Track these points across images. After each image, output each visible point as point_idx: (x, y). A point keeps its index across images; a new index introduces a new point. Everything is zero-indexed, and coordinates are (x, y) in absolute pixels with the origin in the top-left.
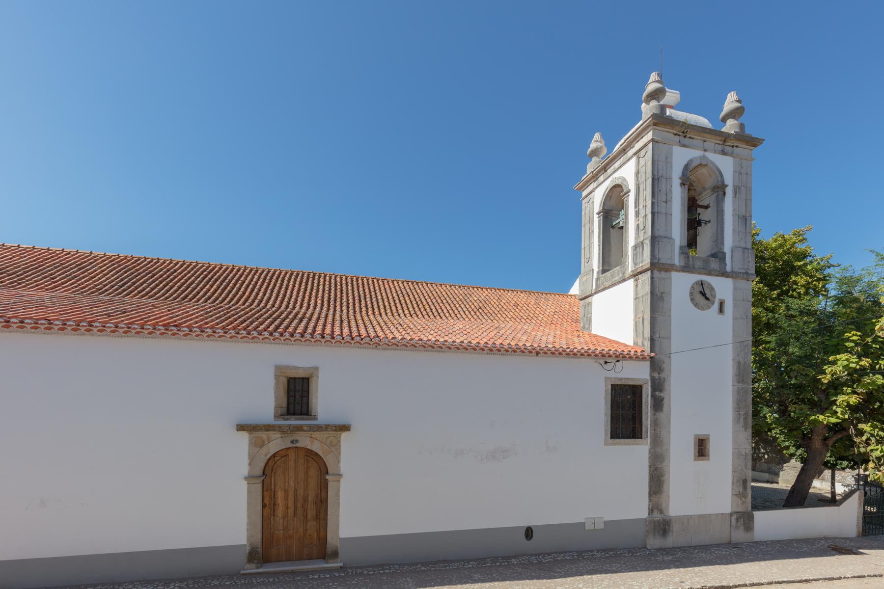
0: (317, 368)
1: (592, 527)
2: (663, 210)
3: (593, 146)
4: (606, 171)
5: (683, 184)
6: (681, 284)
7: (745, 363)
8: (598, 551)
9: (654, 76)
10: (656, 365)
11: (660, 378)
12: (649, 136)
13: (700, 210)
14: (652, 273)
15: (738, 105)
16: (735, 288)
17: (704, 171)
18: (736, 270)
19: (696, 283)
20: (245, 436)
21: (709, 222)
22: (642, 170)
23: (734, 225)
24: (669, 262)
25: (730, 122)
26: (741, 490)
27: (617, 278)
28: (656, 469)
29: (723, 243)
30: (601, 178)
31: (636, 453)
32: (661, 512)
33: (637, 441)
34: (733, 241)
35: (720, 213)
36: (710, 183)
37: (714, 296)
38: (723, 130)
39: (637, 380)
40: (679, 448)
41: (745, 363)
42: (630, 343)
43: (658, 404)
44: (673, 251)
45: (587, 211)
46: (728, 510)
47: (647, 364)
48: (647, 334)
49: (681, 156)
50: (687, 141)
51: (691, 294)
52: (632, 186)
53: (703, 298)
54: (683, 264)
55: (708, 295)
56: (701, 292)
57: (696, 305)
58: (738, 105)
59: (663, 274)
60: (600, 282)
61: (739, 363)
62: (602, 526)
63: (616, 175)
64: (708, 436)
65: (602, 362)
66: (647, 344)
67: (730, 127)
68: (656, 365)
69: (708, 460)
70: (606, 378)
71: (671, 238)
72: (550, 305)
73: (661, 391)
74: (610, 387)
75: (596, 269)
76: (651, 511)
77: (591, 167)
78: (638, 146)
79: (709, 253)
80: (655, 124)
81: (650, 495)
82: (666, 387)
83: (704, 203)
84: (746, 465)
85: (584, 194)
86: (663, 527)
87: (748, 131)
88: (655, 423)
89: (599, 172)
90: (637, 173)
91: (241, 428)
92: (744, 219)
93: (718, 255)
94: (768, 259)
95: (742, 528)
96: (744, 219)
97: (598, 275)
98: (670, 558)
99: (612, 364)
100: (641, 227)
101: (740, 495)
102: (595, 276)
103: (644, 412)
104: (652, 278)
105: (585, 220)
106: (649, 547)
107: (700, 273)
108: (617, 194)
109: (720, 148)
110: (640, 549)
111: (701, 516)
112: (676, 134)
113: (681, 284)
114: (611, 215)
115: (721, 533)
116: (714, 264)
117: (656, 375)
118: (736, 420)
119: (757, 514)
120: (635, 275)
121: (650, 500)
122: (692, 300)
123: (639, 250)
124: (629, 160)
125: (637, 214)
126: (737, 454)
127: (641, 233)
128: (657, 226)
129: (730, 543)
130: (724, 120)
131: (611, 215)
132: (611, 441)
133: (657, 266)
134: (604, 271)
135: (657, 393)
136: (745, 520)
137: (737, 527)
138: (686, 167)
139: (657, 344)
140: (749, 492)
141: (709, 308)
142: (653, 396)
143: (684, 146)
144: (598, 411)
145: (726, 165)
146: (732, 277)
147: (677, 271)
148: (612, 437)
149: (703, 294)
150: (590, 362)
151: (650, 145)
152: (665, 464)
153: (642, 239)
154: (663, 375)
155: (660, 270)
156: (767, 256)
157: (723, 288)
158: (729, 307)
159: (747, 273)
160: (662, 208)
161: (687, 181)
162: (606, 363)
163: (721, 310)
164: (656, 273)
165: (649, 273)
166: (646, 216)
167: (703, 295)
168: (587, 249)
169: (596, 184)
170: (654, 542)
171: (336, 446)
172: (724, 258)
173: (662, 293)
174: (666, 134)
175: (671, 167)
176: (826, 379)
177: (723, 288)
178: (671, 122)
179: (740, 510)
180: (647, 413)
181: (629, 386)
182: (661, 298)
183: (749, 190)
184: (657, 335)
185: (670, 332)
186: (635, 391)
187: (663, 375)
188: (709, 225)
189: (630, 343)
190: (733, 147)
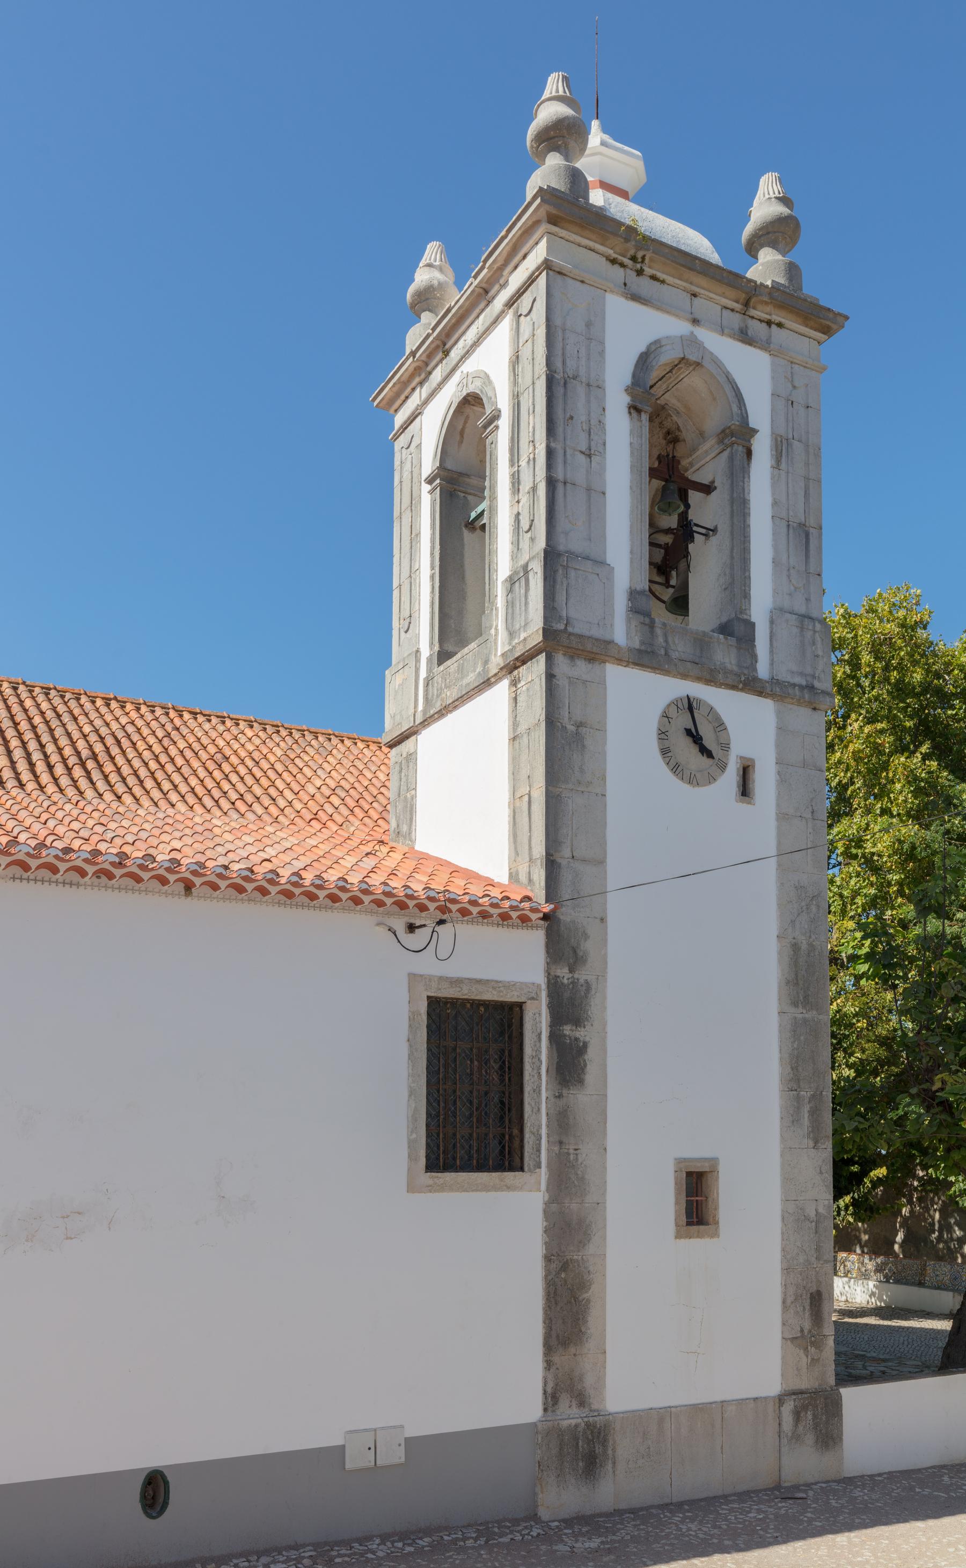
1: (367, 1460)
2: (580, 477)
3: (422, 277)
4: (446, 353)
5: (634, 409)
6: (634, 700)
7: (812, 947)
8: (384, 1538)
9: (554, 84)
10: (564, 942)
11: (574, 983)
12: (538, 254)
13: (694, 497)
14: (549, 660)
15: (782, 210)
16: (782, 729)
17: (693, 381)
18: (784, 676)
19: (675, 703)
21: (714, 530)
22: (526, 353)
23: (775, 547)
24: (596, 632)
25: (767, 255)
26: (807, 1325)
27: (471, 678)
28: (565, 1267)
29: (746, 596)
30: (437, 375)
31: (506, 1215)
32: (582, 1400)
33: (509, 1176)
34: (775, 592)
35: (739, 507)
36: (714, 420)
37: (726, 747)
38: (750, 274)
39: (509, 986)
42: (502, 877)
43: (570, 1063)
44: (608, 601)
45: (406, 475)
46: (772, 1386)
47: (536, 938)
48: (539, 850)
49: (631, 329)
50: (644, 285)
51: (662, 734)
52: (504, 403)
53: (694, 750)
54: (636, 644)
55: (708, 742)
56: (688, 732)
57: (676, 769)
58: (782, 210)
59: (582, 668)
60: (433, 691)
61: (795, 947)
62: (399, 1456)
63: (469, 367)
64: (714, 1162)
65: (399, 925)
66: (539, 875)
67: (766, 268)
68: (564, 942)
69: (715, 1234)
70: (413, 978)
71: (602, 563)
72: (330, 767)
73: (578, 1022)
74: (423, 1007)
75: (425, 652)
76: (551, 1400)
77: (416, 336)
78: (516, 279)
79: (715, 624)
80: (553, 220)
81: (548, 1349)
82: (594, 1009)
83: (703, 477)
84: (818, 1249)
85: (399, 419)
86: (583, 1445)
87: (811, 288)
88: (563, 1122)
89: (430, 355)
90: (515, 360)
92: (802, 536)
93: (737, 630)
94: (955, 695)
95: (810, 1439)
96: (802, 536)
97: (430, 670)
98: (594, 1543)
99: (428, 930)
100: (525, 524)
101: (803, 1340)
102: (423, 674)
103: (528, 1089)
104: (550, 676)
105: (400, 499)
106: (544, 1514)
107: (684, 676)
109: (735, 320)
110: (516, 1522)
111: (698, 1410)
112: (613, 261)
113: (634, 700)
114: (460, 489)
115: (752, 1457)
116: (724, 655)
117: (563, 972)
118: (791, 1117)
119: (849, 1394)
120: (514, 666)
121: (549, 1364)
122: (665, 752)
123: (519, 589)
124: (496, 321)
128: (562, 524)
129: (778, 1487)
130: (752, 249)
131: (460, 489)
132: (428, 1178)
133: (560, 641)
134: (443, 656)
135: (567, 1030)
136: (816, 1412)
137: (796, 1438)
138: (644, 361)
139: (566, 877)
140: (829, 1330)
141: (712, 779)
142: (555, 1037)
143: (635, 298)
144: (382, 1085)
145: (752, 372)
146: (771, 696)
147: (619, 661)
148: (433, 1166)
149: (694, 736)
150: (361, 927)
151: (542, 280)
152: (591, 1249)
153: (525, 557)
154: (582, 975)
155: (573, 654)
156: (950, 688)
157: (750, 725)
158: (765, 781)
159: (811, 688)
160: (577, 469)
161: (647, 400)
162: (411, 928)
163: (745, 790)
164: (561, 660)
165: (542, 658)
166: (534, 489)
167: (693, 740)
168: (405, 588)
169: (425, 391)
170: (560, 1498)
172: (752, 640)
173: (580, 725)
174: (586, 256)
175: (602, 353)
177: (750, 725)
178: (599, 224)
179: (805, 1383)
180: (537, 1091)
181: (486, 1004)
182: (577, 740)
183: (814, 453)
184: (566, 852)
185: (603, 844)
186: (505, 1018)
187: (582, 975)
188: (714, 540)
189: (502, 877)
190: (769, 323)
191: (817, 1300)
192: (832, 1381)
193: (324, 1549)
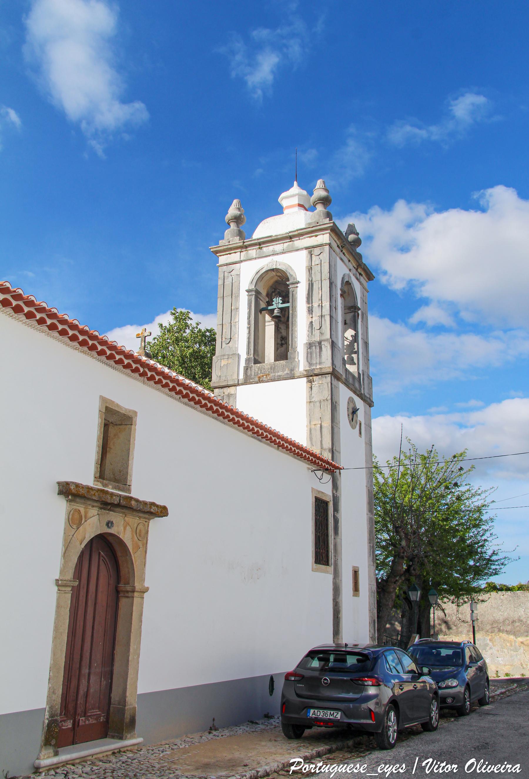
0: (100, 396)
43: (336, 509)
45: (228, 282)
75: (244, 356)
90: (310, 269)
100: (316, 326)
102: (243, 364)
108: (276, 288)
125: (310, 311)
127: (317, 333)
176: (393, 622)
191: (335, 486)
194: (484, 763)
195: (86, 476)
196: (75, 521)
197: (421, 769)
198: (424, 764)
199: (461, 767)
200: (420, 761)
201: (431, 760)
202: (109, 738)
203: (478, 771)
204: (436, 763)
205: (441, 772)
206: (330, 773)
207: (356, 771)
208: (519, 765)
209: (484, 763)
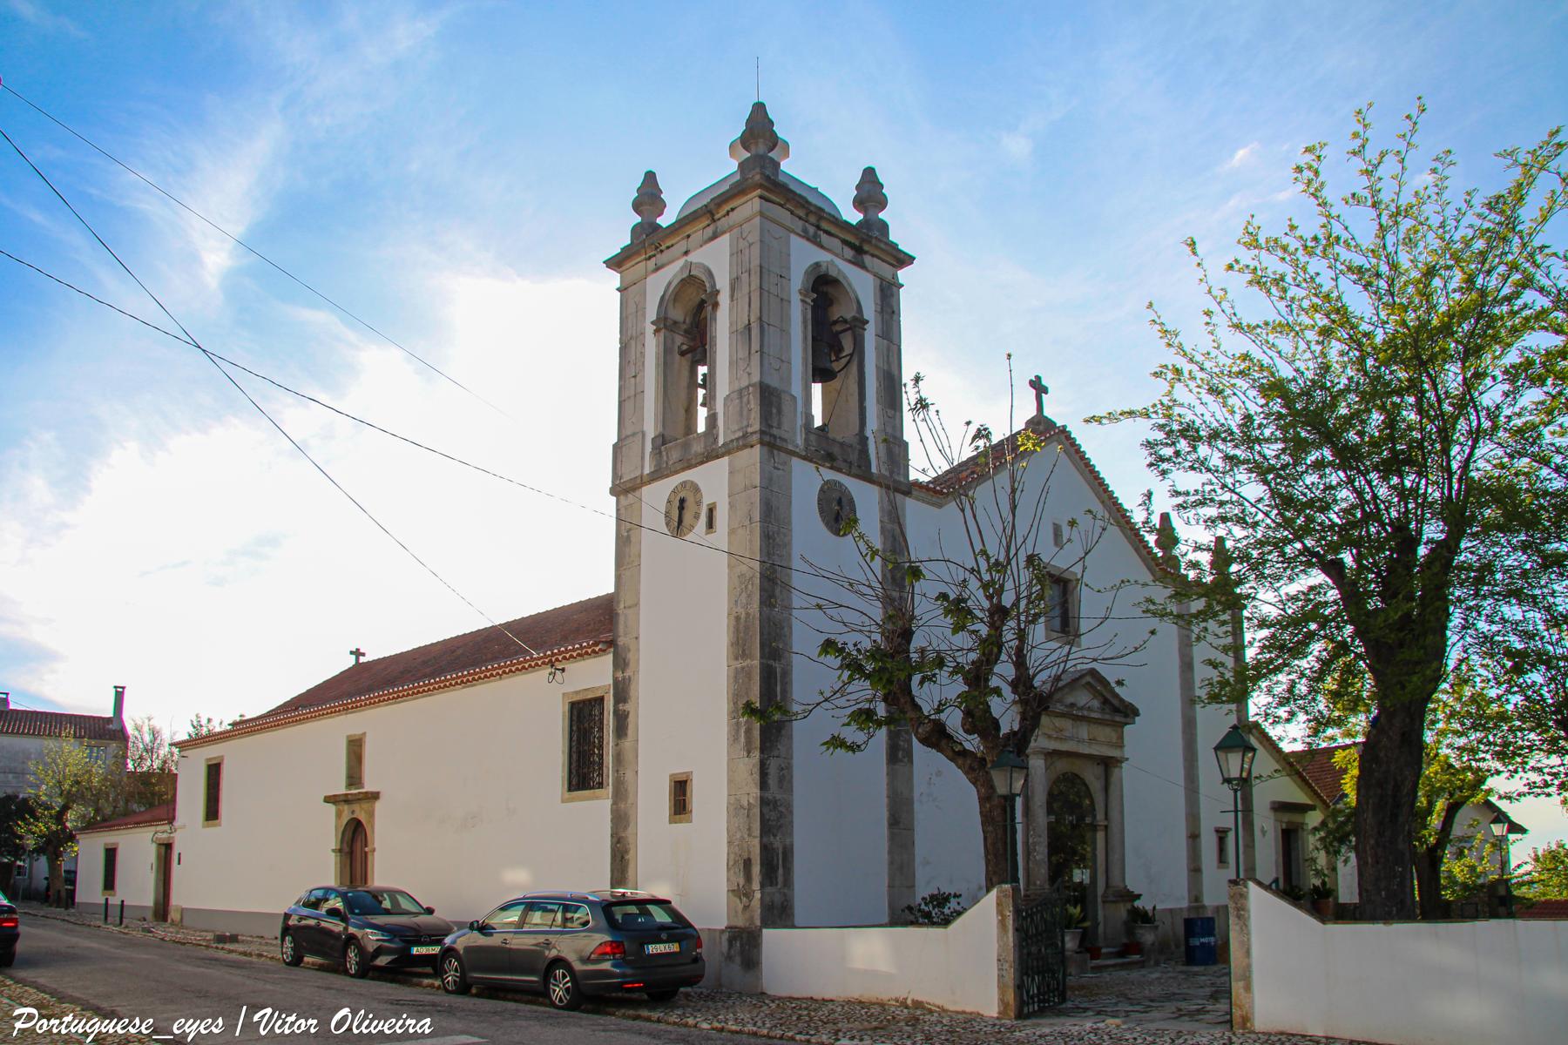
20: (332, 808)
31: (597, 808)
40: (651, 799)
41: (748, 614)
61: (738, 618)
73: (625, 701)
82: (632, 693)
88: (619, 758)
91: (328, 800)
95: (738, 959)
117: (620, 675)
126: (735, 808)
135: (621, 707)
142: (616, 712)
152: (630, 830)
163: (710, 524)
171: (371, 814)
179: (740, 922)
191: (620, 663)
192: (758, 923)
193: (1352, 1042)
194: (366, 1017)
195: (341, 789)
196: (339, 815)
197: (251, 1026)
198: (256, 1018)
199: (324, 1023)
200: (249, 1016)
201: (269, 1011)
202: (759, 978)
203: (356, 1031)
204: (279, 1017)
205: (287, 1032)
206: (86, 1035)
207: (133, 1031)
208: (428, 1020)
209: (366, 1017)
